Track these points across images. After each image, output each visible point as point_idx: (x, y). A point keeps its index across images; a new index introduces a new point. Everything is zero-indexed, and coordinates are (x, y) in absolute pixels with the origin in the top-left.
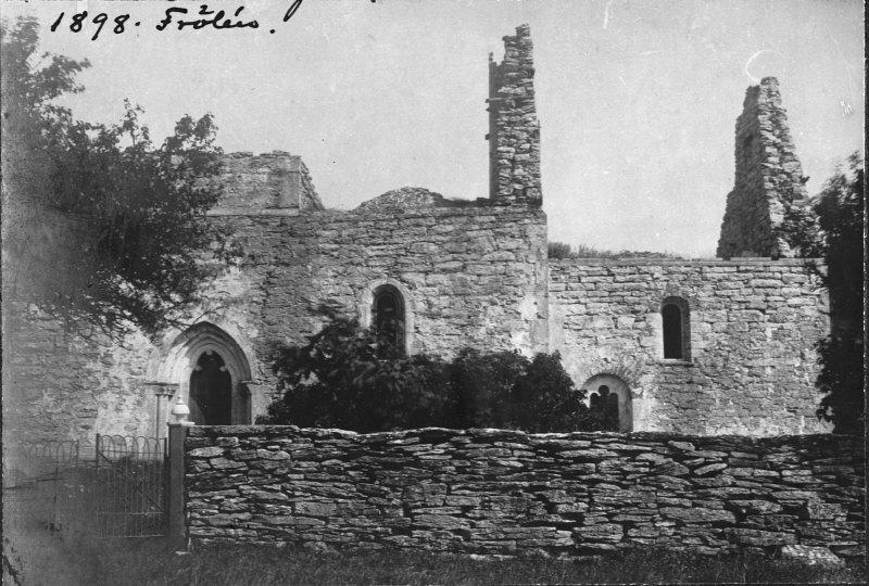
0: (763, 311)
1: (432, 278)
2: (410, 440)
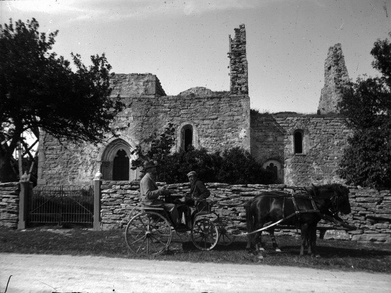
0: (334, 135)
1: (206, 122)
2: (185, 187)
